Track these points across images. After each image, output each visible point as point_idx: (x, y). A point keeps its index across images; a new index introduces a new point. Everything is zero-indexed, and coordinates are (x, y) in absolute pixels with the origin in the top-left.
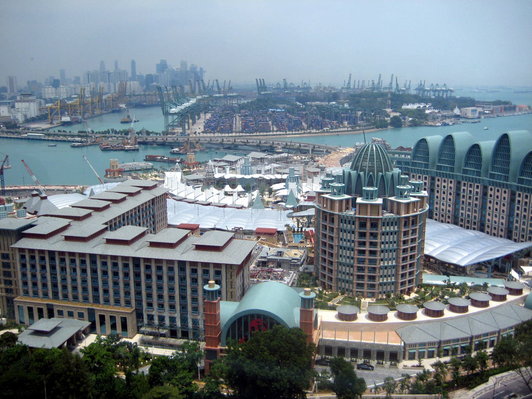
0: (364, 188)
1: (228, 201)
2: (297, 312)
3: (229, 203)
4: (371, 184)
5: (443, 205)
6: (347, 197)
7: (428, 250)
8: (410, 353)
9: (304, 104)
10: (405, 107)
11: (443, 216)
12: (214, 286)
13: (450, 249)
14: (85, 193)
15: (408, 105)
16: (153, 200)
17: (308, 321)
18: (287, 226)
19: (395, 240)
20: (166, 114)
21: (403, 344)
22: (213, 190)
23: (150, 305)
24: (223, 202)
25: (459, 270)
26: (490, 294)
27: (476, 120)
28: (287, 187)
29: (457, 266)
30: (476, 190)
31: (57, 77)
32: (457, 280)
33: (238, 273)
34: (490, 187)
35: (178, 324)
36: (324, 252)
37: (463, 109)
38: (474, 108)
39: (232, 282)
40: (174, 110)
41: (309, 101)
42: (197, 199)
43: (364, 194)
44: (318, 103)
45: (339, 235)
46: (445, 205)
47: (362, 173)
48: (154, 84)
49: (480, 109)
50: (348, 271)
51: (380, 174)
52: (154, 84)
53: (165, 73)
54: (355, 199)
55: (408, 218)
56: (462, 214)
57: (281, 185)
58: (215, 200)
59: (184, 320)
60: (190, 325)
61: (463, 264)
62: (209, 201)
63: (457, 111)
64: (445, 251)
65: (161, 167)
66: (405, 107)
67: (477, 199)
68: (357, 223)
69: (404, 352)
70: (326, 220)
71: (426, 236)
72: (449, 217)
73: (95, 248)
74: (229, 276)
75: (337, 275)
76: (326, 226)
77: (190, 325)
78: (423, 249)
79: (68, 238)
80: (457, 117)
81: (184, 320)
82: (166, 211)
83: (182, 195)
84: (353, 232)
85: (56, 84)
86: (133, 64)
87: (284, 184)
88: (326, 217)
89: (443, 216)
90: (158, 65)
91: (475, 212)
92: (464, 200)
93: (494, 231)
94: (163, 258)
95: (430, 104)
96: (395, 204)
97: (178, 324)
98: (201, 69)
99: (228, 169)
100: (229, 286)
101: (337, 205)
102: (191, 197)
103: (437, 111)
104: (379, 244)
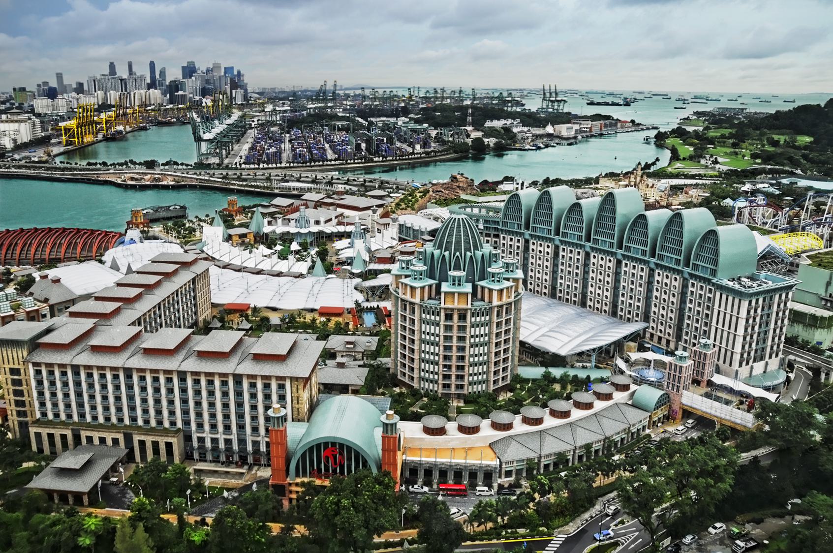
0: (449, 273)
1: (282, 266)
2: (379, 432)
3: (284, 270)
4: (457, 267)
5: (539, 272)
6: (431, 282)
7: (524, 335)
8: (506, 472)
9: (367, 121)
10: (488, 124)
11: (538, 285)
12: (280, 412)
13: (549, 334)
14: (103, 258)
15: (492, 121)
16: (194, 280)
17: (391, 442)
18: (357, 302)
19: (487, 332)
20: (198, 139)
21: (498, 463)
22: (263, 249)
23: (200, 426)
24: (277, 269)
25: (557, 360)
26: (595, 393)
27: (573, 141)
28: (351, 246)
29: (555, 356)
30: (577, 257)
31: (54, 84)
32: (557, 372)
33: (304, 387)
34: (592, 254)
35: (235, 447)
36: (404, 337)
37: (556, 126)
38: (569, 125)
39: (298, 398)
40: (207, 136)
41: (373, 117)
42: (245, 265)
43: (450, 279)
44: (384, 119)
45: (421, 327)
46: (541, 274)
47: (447, 254)
48: (180, 93)
49: (577, 127)
50: (432, 370)
51: (469, 254)
52: (180, 93)
53: (193, 78)
54: (438, 287)
55: (501, 306)
56: (561, 284)
57: (344, 243)
58: (266, 265)
59: (242, 441)
60: (250, 448)
61: (563, 352)
62: (260, 267)
63: (549, 129)
64: (543, 335)
65: (196, 217)
66: (488, 124)
67: (577, 267)
68: (442, 314)
69: (500, 471)
70: (405, 309)
71: (523, 315)
72: (546, 287)
73: (130, 360)
74: (294, 389)
75: (420, 373)
76: (405, 317)
77: (250, 448)
78: (517, 328)
79: (96, 349)
80: (550, 136)
81: (242, 441)
82: (208, 281)
83: (226, 259)
84: (438, 325)
85: (52, 94)
86: (152, 65)
87: (349, 240)
88: (405, 305)
89: (538, 285)
90: (183, 68)
91: (576, 282)
92: (563, 268)
93: (597, 305)
94: (215, 371)
95: (518, 120)
96: (486, 290)
97: (235, 447)
98: (239, 72)
99: (279, 221)
100: (295, 402)
101: (418, 292)
102: (237, 262)
103: (526, 129)
104: (468, 337)
